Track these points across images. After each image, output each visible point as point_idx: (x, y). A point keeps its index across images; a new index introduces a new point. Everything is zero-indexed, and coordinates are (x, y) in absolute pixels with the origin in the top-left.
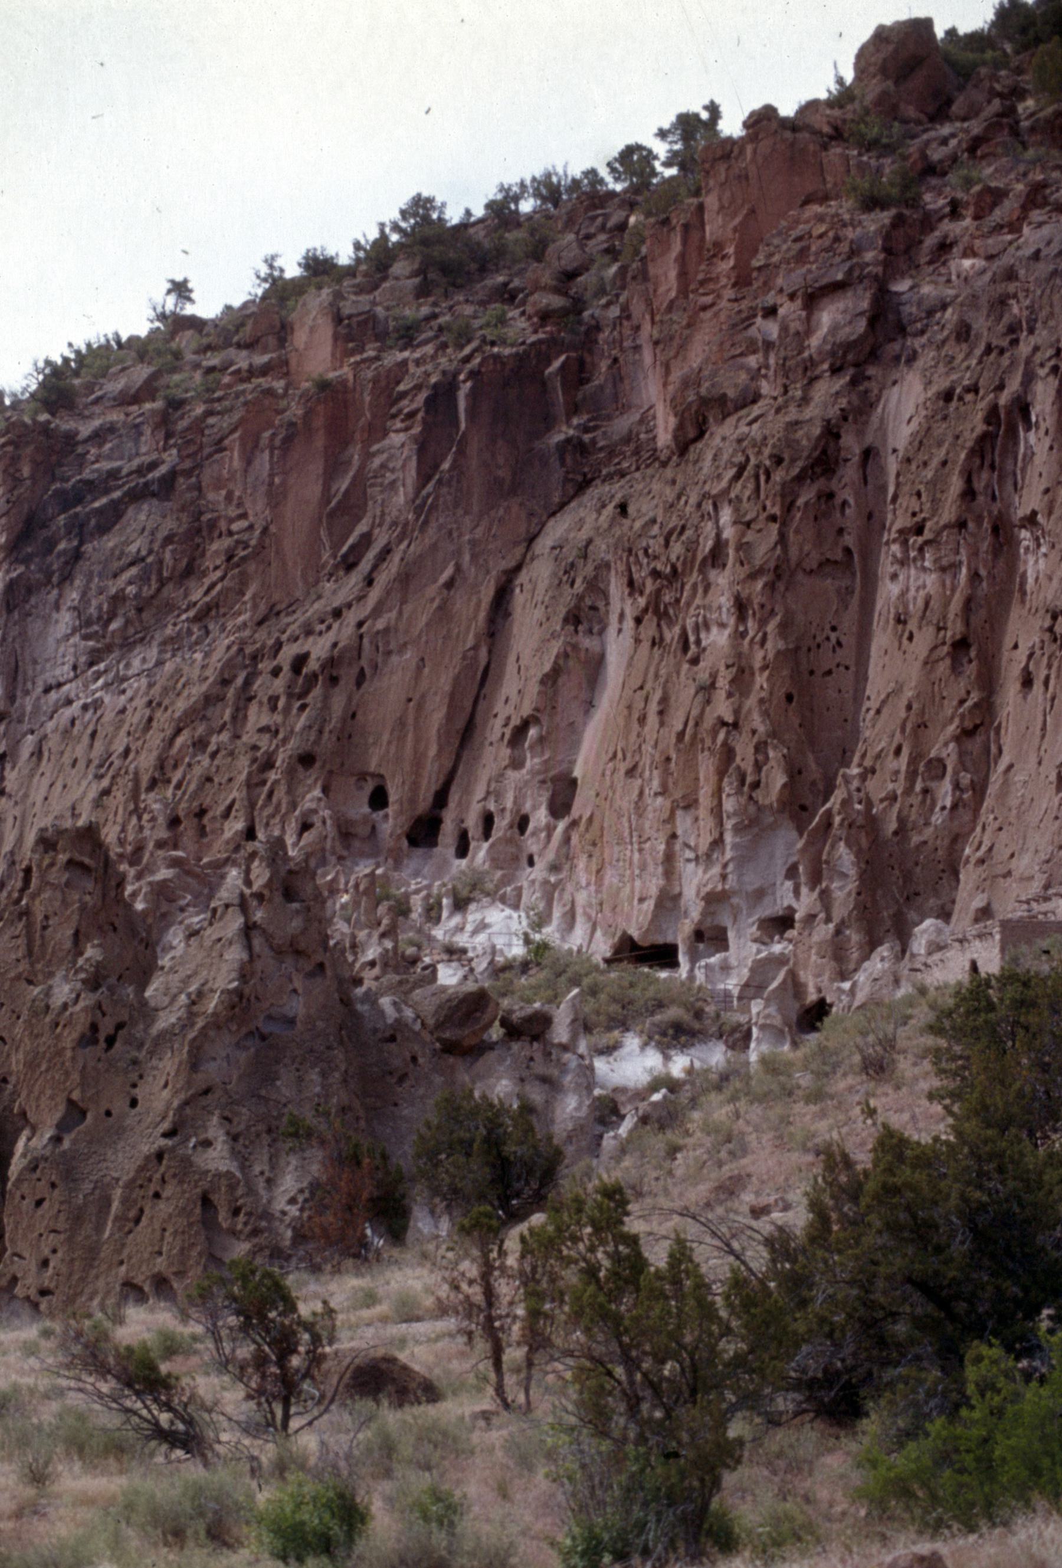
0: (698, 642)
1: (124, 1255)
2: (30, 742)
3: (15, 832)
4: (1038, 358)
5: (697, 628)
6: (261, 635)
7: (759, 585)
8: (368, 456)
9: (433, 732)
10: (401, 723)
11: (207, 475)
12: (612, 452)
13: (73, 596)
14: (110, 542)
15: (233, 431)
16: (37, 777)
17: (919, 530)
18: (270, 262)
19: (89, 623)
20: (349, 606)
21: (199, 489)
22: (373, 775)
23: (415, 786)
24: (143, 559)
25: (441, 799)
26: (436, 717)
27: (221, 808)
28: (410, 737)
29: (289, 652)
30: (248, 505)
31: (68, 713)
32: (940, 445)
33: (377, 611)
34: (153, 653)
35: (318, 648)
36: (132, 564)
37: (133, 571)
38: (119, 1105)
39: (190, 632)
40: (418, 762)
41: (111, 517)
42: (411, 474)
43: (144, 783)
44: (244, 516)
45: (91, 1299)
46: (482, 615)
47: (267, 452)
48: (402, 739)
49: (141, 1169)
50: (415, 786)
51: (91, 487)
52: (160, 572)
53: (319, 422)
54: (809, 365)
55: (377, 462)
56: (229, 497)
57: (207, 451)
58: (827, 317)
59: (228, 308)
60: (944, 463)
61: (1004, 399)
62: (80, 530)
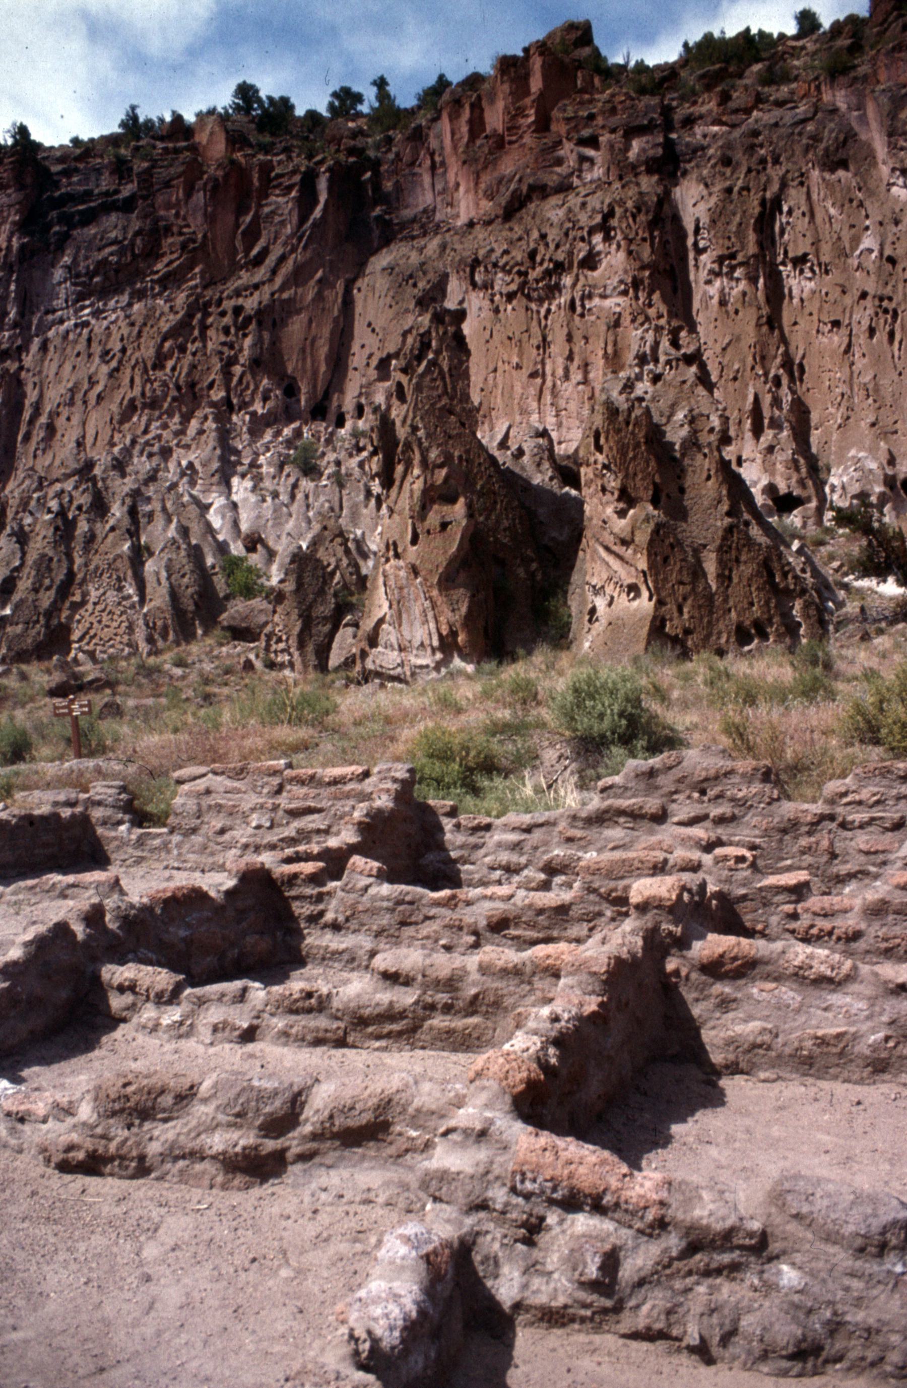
0: (583, 306)
1: (731, 603)
2: (37, 341)
3: (36, 392)
4: (790, 176)
5: (582, 299)
6: (208, 294)
7: (647, 273)
8: (260, 206)
9: (323, 357)
10: (303, 350)
11: (160, 199)
12: (403, 225)
13: (67, 259)
14: (92, 230)
15: (179, 177)
16: (46, 363)
17: (733, 256)
18: (133, 108)
19: (78, 276)
20: (263, 283)
21: (153, 205)
22: (289, 377)
23: (315, 387)
24: (120, 242)
25: (327, 396)
26: (323, 351)
27: (206, 384)
28: (309, 361)
29: (228, 305)
30: (190, 220)
31: (63, 328)
32: (734, 214)
33: (282, 289)
34: (125, 298)
35: (250, 304)
36: (111, 244)
37: (114, 248)
38: (675, 494)
39: (153, 289)
40: (315, 373)
41: (89, 218)
42: (295, 219)
43: (149, 366)
44: (188, 226)
45: (719, 638)
46: (340, 300)
47: (201, 193)
48: (304, 359)
49: (724, 539)
50: (315, 387)
51: (71, 198)
52: (133, 250)
53: (232, 181)
54: (634, 167)
55: (267, 210)
56: (177, 215)
57: (156, 187)
58: (636, 145)
59: (76, 141)
60: (740, 224)
61: (768, 195)
62: (68, 220)
